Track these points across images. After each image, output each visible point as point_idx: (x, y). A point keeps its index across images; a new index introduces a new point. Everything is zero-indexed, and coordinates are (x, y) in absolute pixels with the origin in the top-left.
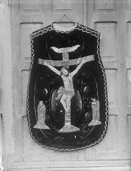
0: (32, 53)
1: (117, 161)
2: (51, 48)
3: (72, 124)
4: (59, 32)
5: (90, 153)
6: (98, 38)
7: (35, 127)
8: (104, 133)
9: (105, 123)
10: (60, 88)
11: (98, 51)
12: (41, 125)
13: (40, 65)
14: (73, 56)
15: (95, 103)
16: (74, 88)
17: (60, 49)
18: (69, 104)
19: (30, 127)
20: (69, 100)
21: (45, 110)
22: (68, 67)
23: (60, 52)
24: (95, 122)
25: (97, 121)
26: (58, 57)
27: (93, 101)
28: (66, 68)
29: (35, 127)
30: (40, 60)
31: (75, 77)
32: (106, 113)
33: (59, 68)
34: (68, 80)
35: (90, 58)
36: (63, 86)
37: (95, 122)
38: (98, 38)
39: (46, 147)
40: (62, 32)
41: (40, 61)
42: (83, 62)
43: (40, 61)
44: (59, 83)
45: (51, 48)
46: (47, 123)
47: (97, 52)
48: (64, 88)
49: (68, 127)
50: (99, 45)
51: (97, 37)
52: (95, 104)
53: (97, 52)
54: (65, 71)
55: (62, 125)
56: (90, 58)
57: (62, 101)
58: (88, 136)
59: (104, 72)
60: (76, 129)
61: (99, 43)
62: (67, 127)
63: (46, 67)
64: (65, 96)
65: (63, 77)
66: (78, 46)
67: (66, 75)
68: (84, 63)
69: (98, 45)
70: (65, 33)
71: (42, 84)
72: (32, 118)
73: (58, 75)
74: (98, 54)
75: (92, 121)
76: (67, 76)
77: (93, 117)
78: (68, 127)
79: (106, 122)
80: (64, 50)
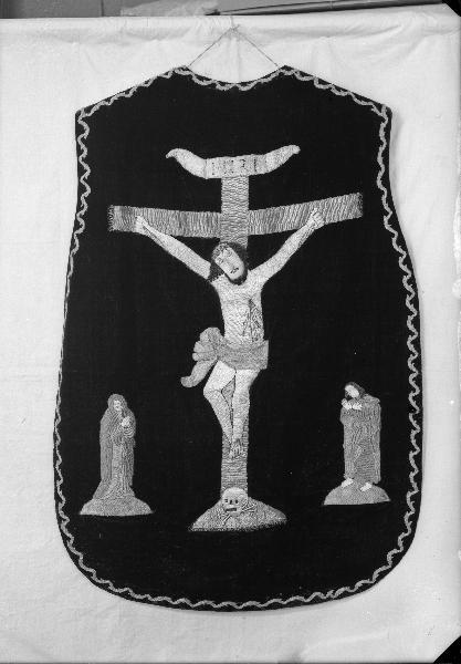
0: (82, 181)
1: (100, 6)
2: (170, 154)
3: (252, 493)
4: (210, 82)
5: (330, 626)
6: (384, 121)
7: (88, 509)
8: (400, 543)
9: (408, 500)
10: (204, 336)
11: (381, 174)
12: (115, 497)
13: (117, 233)
14: (264, 192)
15: (357, 407)
16: (265, 338)
17: (210, 161)
18: (242, 407)
19: (63, 509)
20: (243, 388)
21: (131, 433)
22: (245, 243)
23: (209, 176)
24: (357, 488)
25: (368, 486)
26: (207, 195)
27: (349, 398)
28: (234, 247)
29: (88, 509)
30: (117, 211)
31: (270, 290)
32: (411, 454)
33: (204, 247)
34: (240, 301)
35: (344, 207)
36: (219, 323)
37: (357, 488)
38: (384, 121)
39: (150, 598)
40: (218, 87)
41: (118, 218)
42: (310, 222)
43: (118, 218)
44: (212, 314)
45: (170, 154)
46: (140, 488)
47: (379, 183)
48: (223, 332)
49: (236, 507)
50: (387, 147)
51: (379, 114)
52: (358, 410)
53: (379, 183)
54: (229, 261)
55: (211, 494)
56: (344, 207)
57: (211, 392)
58: (333, 550)
59: (411, 290)
60: (270, 516)
61: (388, 141)
62: (232, 506)
63: (146, 243)
64: (228, 372)
65: (220, 284)
66: (295, 149)
67: (234, 276)
68: (316, 227)
69: (382, 149)
70: (235, 88)
71: (125, 321)
72: (77, 468)
73: (201, 278)
74: (383, 139)
75: (345, 484)
76: (240, 281)
77: (349, 467)
78: (236, 507)
79: (409, 495)
80: (228, 167)
